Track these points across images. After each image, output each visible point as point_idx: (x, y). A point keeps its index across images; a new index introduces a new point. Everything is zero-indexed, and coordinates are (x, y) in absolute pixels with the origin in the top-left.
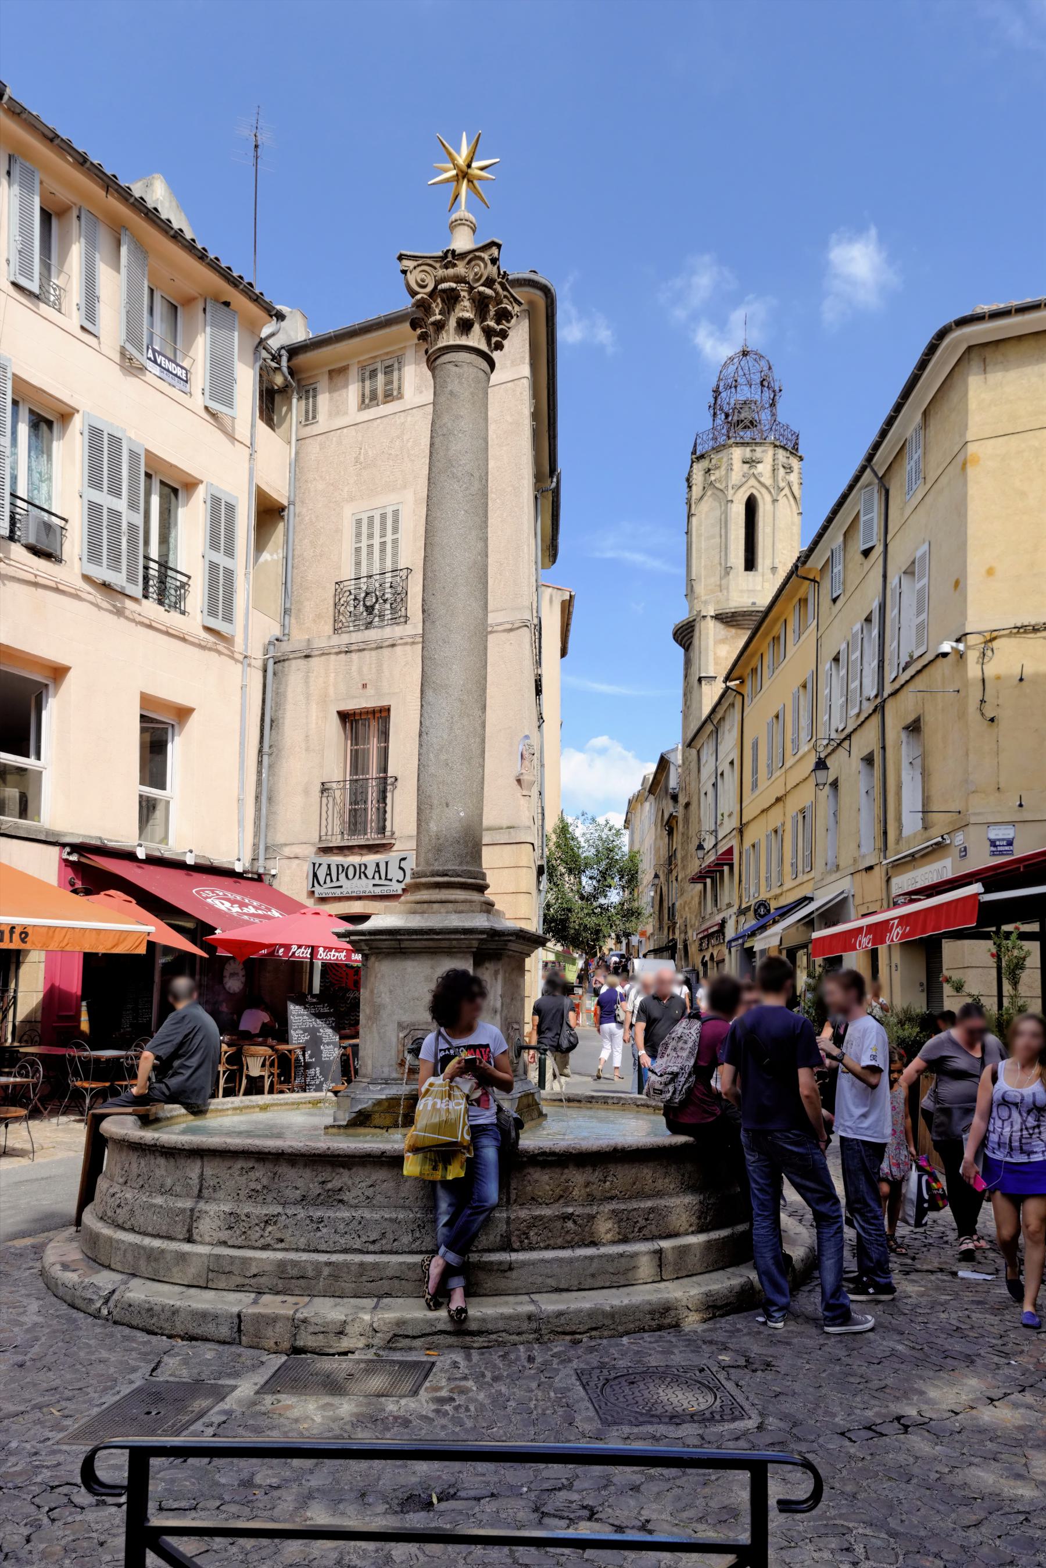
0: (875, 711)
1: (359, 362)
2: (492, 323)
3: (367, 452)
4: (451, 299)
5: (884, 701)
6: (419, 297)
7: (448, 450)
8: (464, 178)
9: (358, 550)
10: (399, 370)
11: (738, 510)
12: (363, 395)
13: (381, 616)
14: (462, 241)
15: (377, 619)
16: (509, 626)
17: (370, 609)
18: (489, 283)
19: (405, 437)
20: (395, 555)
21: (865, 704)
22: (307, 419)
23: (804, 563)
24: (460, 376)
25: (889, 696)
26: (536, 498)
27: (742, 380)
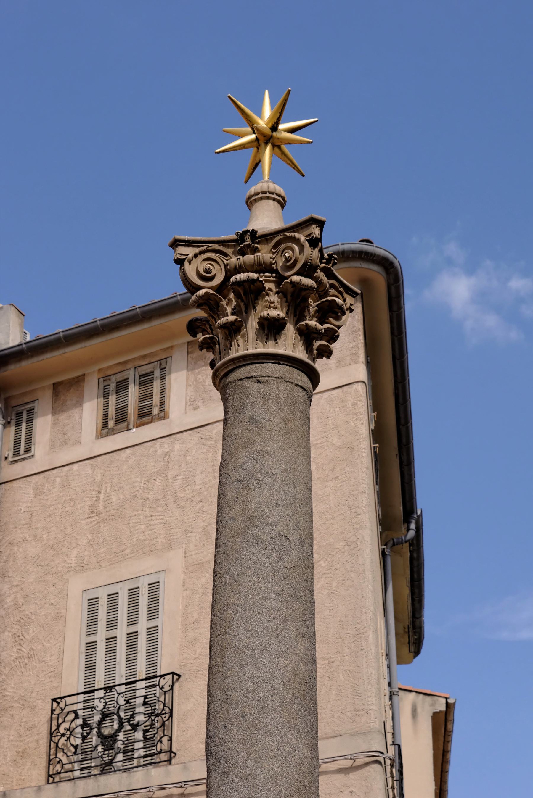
1: (100, 370)
2: (313, 323)
3: (108, 497)
4: (251, 293)
6: (202, 292)
7: (247, 502)
8: (266, 144)
9: (91, 646)
10: (163, 378)
12: (106, 416)
13: (128, 752)
14: (266, 219)
15: (120, 757)
16: (347, 763)
17: (108, 742)
18: (308, 270)
19: (171, 474)
20: (152, 652)
22: (16, 453)
24: (265, 397)
26: (383, 554)
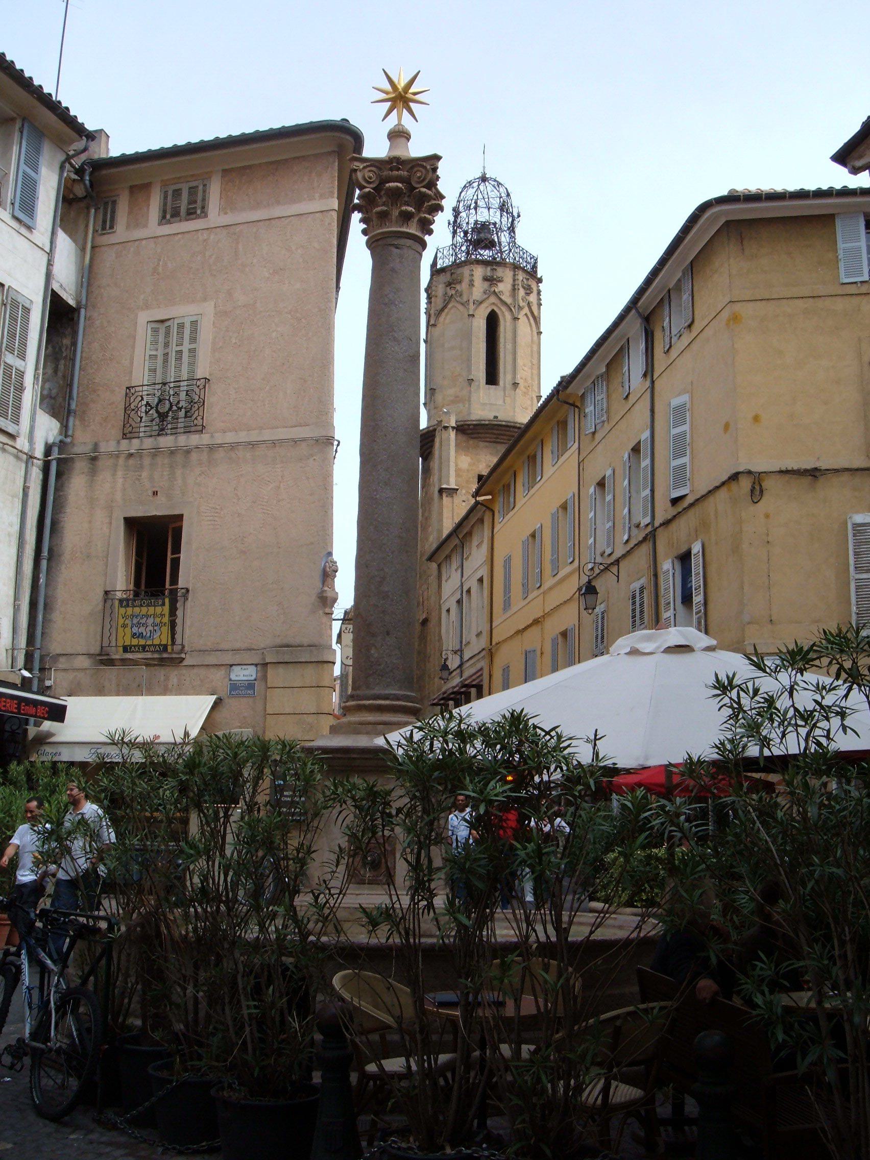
0: (645, 539)
5: (655, 530)
11: (480, 325)
19: (208, 254)
21: (635, 531)
22: (104, 228)
23: (566, 388)
25: (661, 525)
27: (481, 203)
